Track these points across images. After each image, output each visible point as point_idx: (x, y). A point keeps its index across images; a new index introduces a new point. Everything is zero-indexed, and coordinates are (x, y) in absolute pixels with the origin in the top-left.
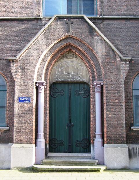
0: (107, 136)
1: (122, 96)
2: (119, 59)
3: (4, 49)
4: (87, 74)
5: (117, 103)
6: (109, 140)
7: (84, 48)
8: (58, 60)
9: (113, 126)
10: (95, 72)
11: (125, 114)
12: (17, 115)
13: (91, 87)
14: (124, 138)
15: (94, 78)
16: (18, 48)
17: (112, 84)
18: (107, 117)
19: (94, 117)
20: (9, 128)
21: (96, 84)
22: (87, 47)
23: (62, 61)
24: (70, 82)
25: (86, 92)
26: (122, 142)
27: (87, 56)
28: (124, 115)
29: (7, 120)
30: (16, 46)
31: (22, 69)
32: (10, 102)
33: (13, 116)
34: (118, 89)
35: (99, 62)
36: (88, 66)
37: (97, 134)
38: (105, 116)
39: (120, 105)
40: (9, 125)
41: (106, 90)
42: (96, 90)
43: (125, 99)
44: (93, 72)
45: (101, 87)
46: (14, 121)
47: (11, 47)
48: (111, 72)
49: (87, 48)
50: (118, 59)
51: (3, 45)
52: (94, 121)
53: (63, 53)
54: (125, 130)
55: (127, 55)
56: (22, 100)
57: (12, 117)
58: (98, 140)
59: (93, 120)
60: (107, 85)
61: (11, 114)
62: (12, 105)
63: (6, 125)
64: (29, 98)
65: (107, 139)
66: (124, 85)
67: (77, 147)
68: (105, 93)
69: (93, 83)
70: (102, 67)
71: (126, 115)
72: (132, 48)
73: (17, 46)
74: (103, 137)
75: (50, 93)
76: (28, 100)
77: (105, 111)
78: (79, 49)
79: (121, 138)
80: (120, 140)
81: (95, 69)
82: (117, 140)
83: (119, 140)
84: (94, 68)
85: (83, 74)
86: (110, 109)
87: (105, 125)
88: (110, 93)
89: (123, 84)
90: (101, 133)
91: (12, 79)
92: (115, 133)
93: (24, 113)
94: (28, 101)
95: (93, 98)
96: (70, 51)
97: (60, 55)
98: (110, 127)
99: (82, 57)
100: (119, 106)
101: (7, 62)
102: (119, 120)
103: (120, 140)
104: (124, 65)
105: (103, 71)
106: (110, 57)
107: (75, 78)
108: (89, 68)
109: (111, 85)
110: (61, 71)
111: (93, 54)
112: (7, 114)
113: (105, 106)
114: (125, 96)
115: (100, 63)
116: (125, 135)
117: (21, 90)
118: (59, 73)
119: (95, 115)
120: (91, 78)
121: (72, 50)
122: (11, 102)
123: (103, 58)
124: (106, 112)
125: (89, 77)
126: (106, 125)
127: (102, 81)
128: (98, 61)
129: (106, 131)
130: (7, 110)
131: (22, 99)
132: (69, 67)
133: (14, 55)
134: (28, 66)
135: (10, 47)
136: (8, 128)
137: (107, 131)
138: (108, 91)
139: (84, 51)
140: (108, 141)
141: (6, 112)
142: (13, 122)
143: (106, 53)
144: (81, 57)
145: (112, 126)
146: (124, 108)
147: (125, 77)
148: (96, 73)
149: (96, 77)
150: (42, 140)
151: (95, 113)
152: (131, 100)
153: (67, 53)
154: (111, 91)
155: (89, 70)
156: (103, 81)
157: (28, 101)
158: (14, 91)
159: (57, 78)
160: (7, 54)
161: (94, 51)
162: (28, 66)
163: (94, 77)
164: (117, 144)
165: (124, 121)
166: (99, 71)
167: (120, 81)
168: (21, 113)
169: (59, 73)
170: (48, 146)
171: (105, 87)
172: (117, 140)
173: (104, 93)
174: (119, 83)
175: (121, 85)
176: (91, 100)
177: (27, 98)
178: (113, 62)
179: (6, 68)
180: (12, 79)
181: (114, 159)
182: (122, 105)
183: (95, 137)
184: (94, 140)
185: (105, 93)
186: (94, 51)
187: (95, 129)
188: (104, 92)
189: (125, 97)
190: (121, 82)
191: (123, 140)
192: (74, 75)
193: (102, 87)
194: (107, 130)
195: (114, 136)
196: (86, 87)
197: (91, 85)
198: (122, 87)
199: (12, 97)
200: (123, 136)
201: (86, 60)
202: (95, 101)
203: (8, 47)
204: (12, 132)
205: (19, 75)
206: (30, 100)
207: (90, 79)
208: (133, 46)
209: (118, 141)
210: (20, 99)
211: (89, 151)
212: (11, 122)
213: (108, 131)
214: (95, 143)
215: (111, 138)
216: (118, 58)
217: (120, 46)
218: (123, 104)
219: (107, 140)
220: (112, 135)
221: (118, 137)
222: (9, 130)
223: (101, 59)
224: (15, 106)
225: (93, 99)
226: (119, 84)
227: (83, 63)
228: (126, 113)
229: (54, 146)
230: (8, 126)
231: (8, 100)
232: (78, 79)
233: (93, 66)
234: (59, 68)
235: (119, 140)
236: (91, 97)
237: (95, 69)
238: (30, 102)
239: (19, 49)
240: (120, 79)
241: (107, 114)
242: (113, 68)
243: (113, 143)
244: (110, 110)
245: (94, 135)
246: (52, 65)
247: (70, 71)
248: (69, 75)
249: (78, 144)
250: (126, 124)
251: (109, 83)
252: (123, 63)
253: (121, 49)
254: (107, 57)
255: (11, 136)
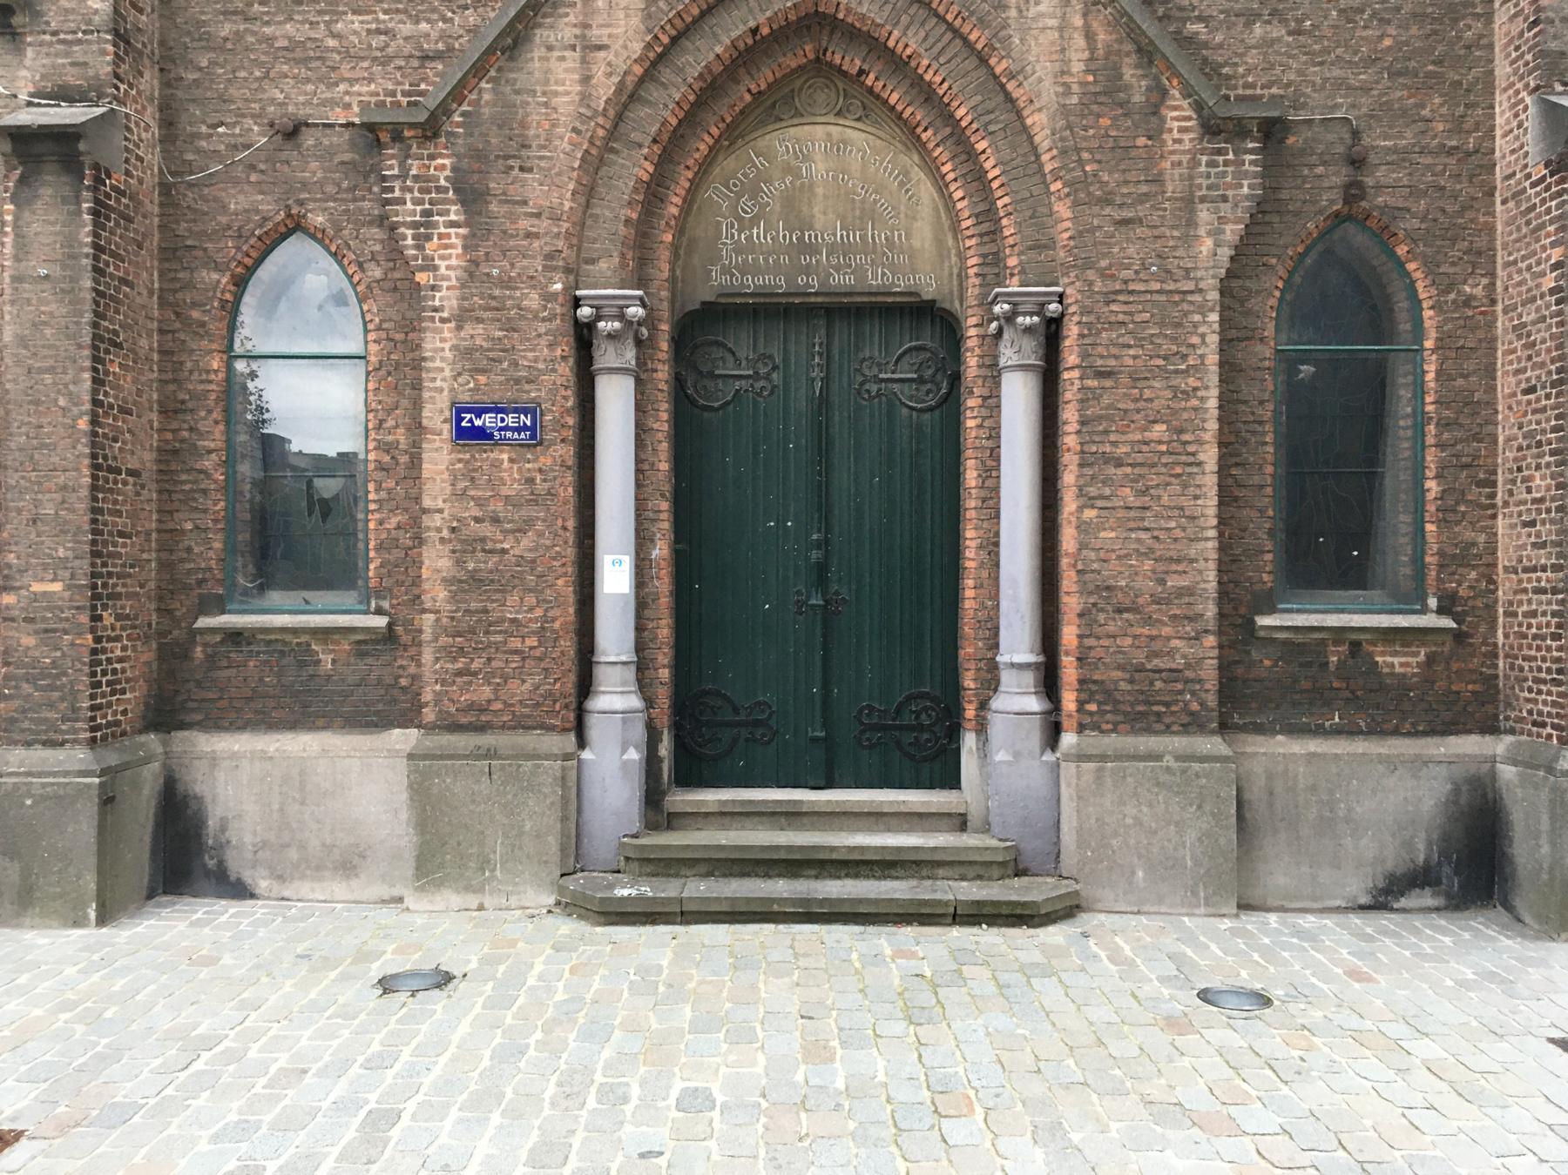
0: (1081, 682)
1: (1202, 399)
2: (1189, 118)
3: (331, 43)
4: (939, 242)
5: (1164, 448)
6: (1093, 707)
7: (925, 39)
8: (734, 134)
9: (1127, 610)
10: (1005, 222)
11: (1214, 522)
12: (445, 533)
13: (972, 332)
14: (1203, 695)
15: (996, 264)
16: (434, 35)
17: (1132, 308)
18: (1083, 546)
19: (992, 546)
20: (390, 625)
21: (1006, 307)
22: (950, 26)
23: (761, 143)
24: (819, 300)
25: (930, 372)
26: (1186, 720)
27: (946, 100)
28: (1212, 533)
29: (372, 566)
30: (417, 22)
31: (471, 195)
32: (390, 438)
33: (419, 541)
34: (1168, 347)
35: (1034, 148)
36: (951, 176)
37: (1013, 665)
38: (1068, 540)
39: (1184, 458)
40: (386, 605)
41: (1084, 355)
42: (1008, 355)
43: (1220, 419)
44: (985, 227)
45: (1042, 330)
46: (425, 573)
47: (379, 32)
48: (1125, 222)
49: (949, 35)
50: (1174, 119)
51: (320, 13)
52: (985, 574)
53: (771, 79)
54: (1211, 640)
55: (1249, 92)
56: (478, 423)
57: (409, 543)
58: (1017, 699)
59: (981, 565)
60: (1092, 318)
61: (398, 527)
62: (404, 459)
63: (369, 603)
64: (525, 411)
65: (1084, 696)
66: (1214, 317)
67: (864, 747)
68: (1076, 374)
69: (987, 304)
70: (1059, 185)
71: (1221, 534)
72: (1290, 33)
73: (424, 26)
74: (1049, 682)
75: (678, 382)
76: (525, 428)
77: (1069, 504)
78: (891, 44)
79: (1181, 692)
80: (1174, 708)
81: (1006, 200)
82: (1155, 708)
83: (1167, 704)
84: (999, 193)
85: (916, 243)
86: (1107, 491)
87: (1065, 599)
88: (1108, 374)
89: (1212, 310)
90: (1041, 659)
91: (397, 275)
92: (1139, 657)
93: (496, 520)
94: (518, 430)
95: (984, 412)
96: (820, 67)
97: (748, 98)
98: (1102, 617)
99: (909, 110)
100: (1178, 470)
101: (353, 145)
102: (1174, 567)
103: (1174, 708)
104: (1226, 163)
105: (1062, 209)
106: (1121, 105)
107: (859, 271)
108: (958, 195)
109: (1121, 317)
110: (754, 221)
111: (991, 84)
112: (372, 525)
113: (1073, 467)
114: (1220, 398)
115: (1040, 151)
116: (1209, 672)
117: (465, 353)
118: (740, 232)
119: (997, 534)
120: (971, 272)
121: (838, 61)
122: (401, 436)
123: (1064, 110)
124: (1081, 509)
125: (954, 259)
126: (1071, 602)
127: (1057, 285)
128: (1030, 138)
129: (1075, 642)
130: (371, 496)
131: (479, 416)
132: (811, 186)
133: (404, 94)
134: (516, 171)
135: (369, 31)
136: (381, 622)
137: (1080, 646)
138: (1099, 362)
139: (925, 62)
140: (1091, 714)
141: (368, 512)
142: (417, 581)
143: (1087, 71)
144: (905, 115)
145: (1120, 611)
146: (1210, 481)
147: (1225, 253)
148: (1008, 227)
149: (1012, 262)
150: (615, 697)
151: (998, 516)
152: (1261, 423)
153: (798, 83)
154: (1116, 357)
155: (959, 205)
156: (1059, 289)
157: (518, 430)
158: (418, 364)
159: (726, 270)
160: (352, 82)
161: (1004, 64)
162: (516, 171)
163: (994, 266)
164: (1156, 733)
165: (1212, 575)
166: (1036, 214)
167: (1190, 286)
168: (477, 520)
169: (740, 232)
170: (665, 749)
171: (1072, 331)
172: (1155, 708)
173: (1066, 375)
174: (1176, 298)
175: (1197, 318)
176: (970, 423)
177: (516, 410)
178: (1142, 141)
179: (352, 189)
180: (397, 275)
181: (1132, 841)
182: (1199, 464)
183: (991, 681)
184: (983, 705)
185: (1076, 374)
186: (1004, 64)
187: (995, 631)
188: (1062, 366)
189: (1220, 407)
190: (1201, 291)
191: (1195, 706)
192: (846, 249)
193: (1052, 332)
194: (1080, 637)
195: (1131, 682)
196: (892, 368)
197: (972, 321)
198: (1202, 330)
199: (405, 403)
200: (1200, 681)
201: (939, 137)
202: (995, 434)
203: (355, 32)
204: (412, 651)
205: (454, 240)
206: (533, 429)
207: (962, 277)
208: (1300, 21)
209: (1158, 714)
210: (1292, 370)
211: (951, 780)
212: (400, 583)
213: (1091, 642)
214: (998, 727)
215: (1108, 693)
216: (1175, 108)
217: (1200, 19)
218: (1201, 457)
219: (1081, 704)
220: (1119, 674)
221: (1158, 685)
222: (389, 637)
223: (1052, 118)
224: (428, 468)
225: (984, 419)
226: (1185, 307)
227: (911, 161)
228: (1222, 522)
229: (701, 738)
230: (379, 611)
231: (379, 427)
232: (876, 278)
233: (990, 176)
234: (739, 195)
235: (1167, 704)
236: (971, 403)
237: (1006, 200)
238: (533, 437)
239: (441, 46)
240: (1187, 270)
241: (1082, 527)
242: (1144, 188)
243: (1128, 727)
244: (1106, 498)
245: (988, 671)
246: (690, 175)
247: (826, 222)
248: (812, 249)
249: (874, 728)
250: (1224, 595)
251: (1108, 303)
252: (1219, 152)
253: (1206, 45)
254: (1095, 107)
255: (403, 682)
